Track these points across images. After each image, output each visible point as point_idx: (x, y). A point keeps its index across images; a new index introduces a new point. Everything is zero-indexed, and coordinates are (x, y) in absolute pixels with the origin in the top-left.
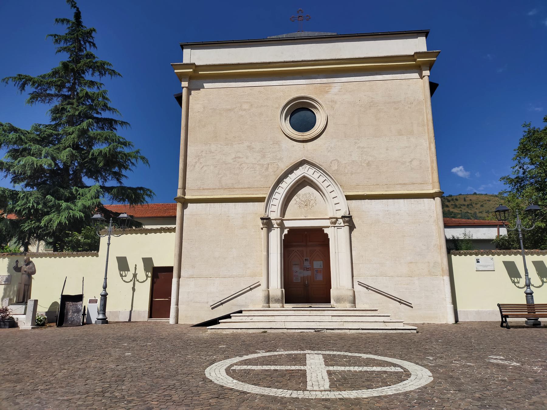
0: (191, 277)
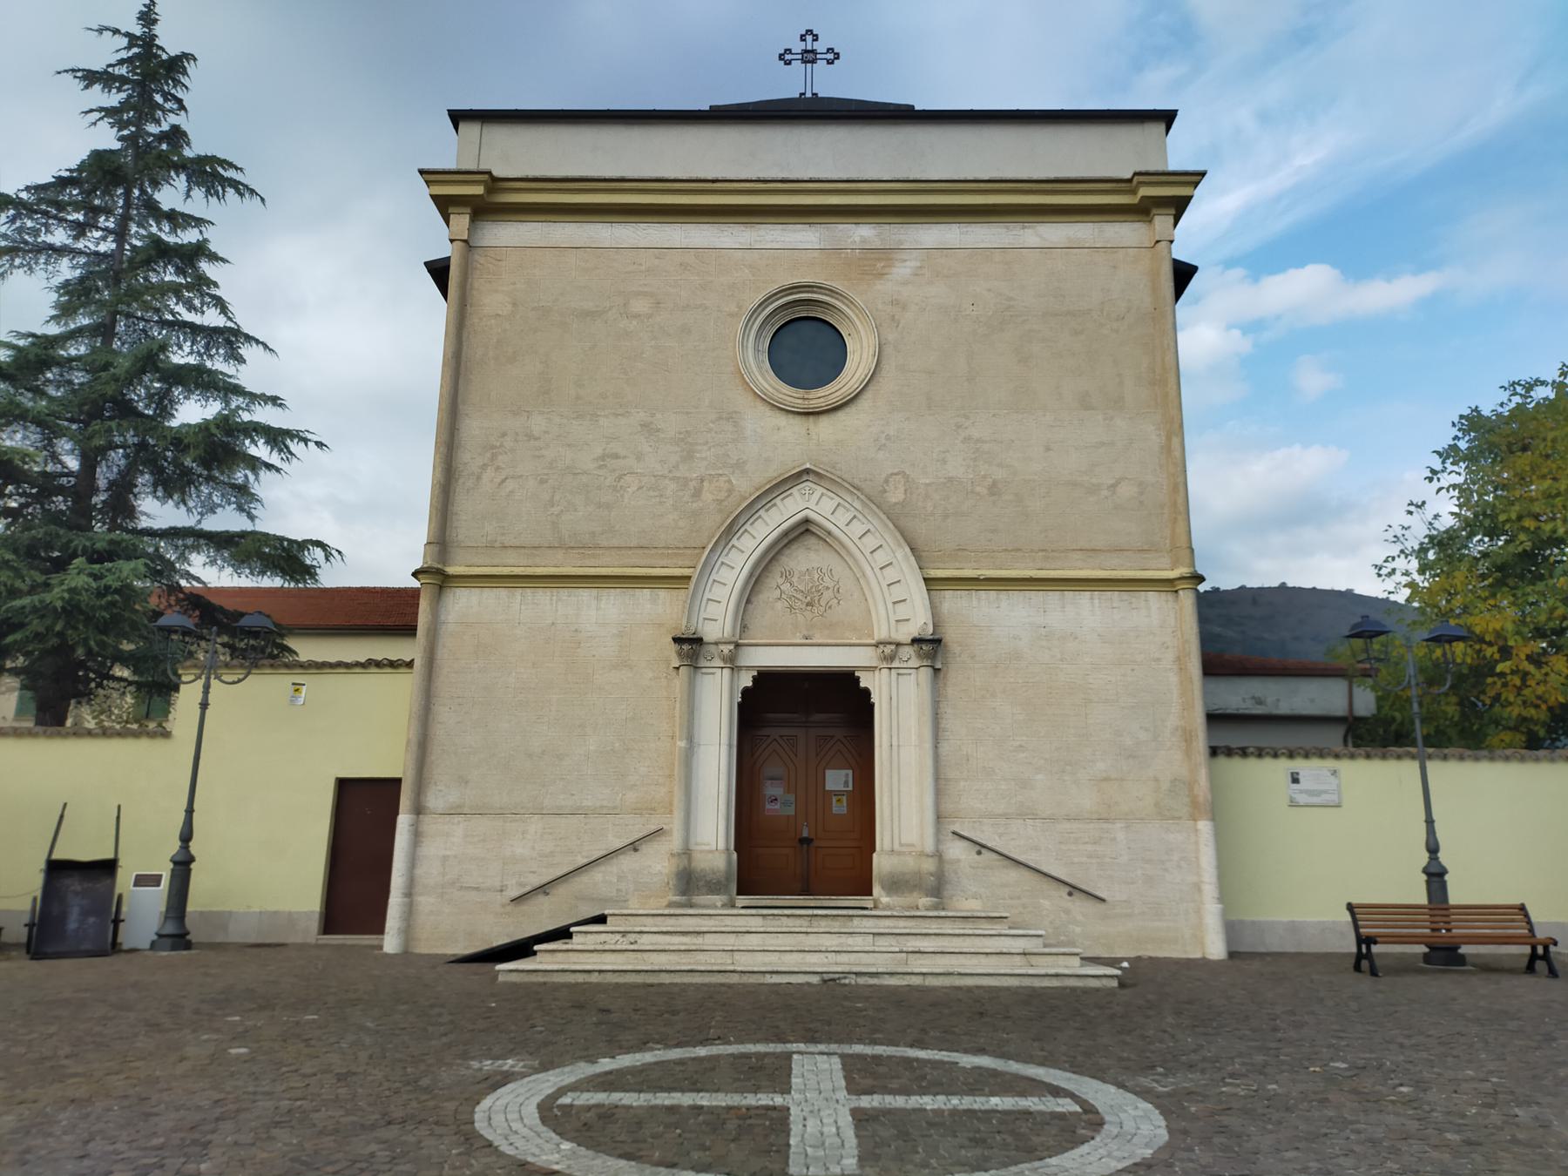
0: (453, 812)
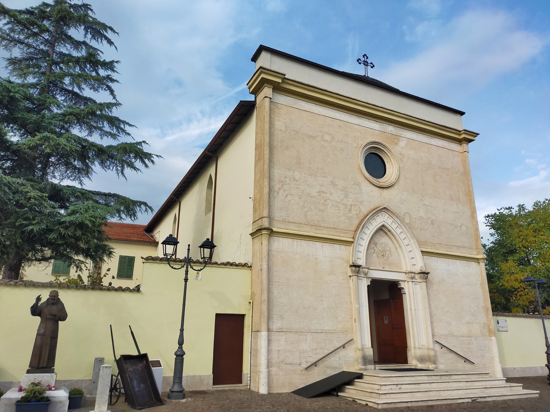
0: (280, 331)
